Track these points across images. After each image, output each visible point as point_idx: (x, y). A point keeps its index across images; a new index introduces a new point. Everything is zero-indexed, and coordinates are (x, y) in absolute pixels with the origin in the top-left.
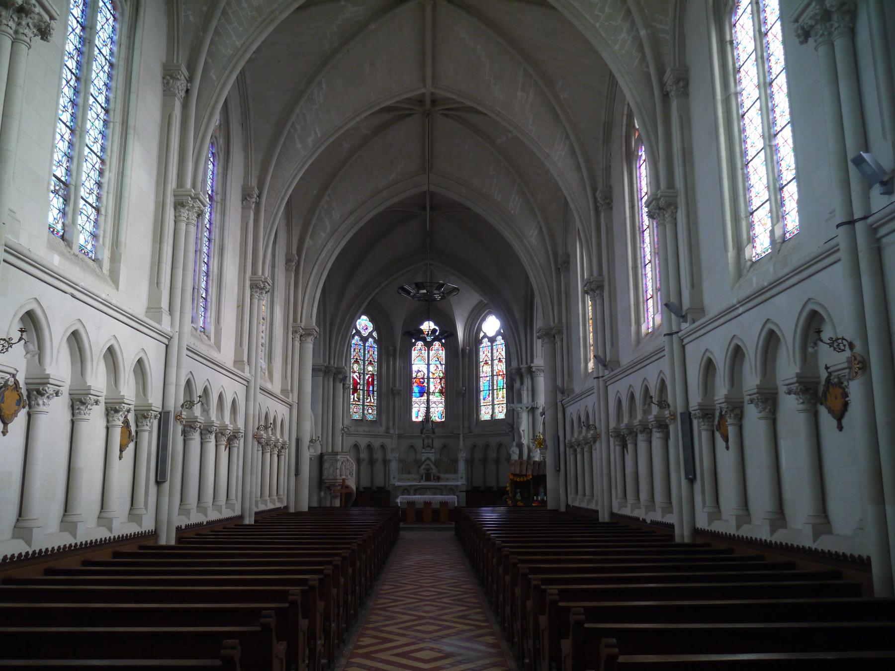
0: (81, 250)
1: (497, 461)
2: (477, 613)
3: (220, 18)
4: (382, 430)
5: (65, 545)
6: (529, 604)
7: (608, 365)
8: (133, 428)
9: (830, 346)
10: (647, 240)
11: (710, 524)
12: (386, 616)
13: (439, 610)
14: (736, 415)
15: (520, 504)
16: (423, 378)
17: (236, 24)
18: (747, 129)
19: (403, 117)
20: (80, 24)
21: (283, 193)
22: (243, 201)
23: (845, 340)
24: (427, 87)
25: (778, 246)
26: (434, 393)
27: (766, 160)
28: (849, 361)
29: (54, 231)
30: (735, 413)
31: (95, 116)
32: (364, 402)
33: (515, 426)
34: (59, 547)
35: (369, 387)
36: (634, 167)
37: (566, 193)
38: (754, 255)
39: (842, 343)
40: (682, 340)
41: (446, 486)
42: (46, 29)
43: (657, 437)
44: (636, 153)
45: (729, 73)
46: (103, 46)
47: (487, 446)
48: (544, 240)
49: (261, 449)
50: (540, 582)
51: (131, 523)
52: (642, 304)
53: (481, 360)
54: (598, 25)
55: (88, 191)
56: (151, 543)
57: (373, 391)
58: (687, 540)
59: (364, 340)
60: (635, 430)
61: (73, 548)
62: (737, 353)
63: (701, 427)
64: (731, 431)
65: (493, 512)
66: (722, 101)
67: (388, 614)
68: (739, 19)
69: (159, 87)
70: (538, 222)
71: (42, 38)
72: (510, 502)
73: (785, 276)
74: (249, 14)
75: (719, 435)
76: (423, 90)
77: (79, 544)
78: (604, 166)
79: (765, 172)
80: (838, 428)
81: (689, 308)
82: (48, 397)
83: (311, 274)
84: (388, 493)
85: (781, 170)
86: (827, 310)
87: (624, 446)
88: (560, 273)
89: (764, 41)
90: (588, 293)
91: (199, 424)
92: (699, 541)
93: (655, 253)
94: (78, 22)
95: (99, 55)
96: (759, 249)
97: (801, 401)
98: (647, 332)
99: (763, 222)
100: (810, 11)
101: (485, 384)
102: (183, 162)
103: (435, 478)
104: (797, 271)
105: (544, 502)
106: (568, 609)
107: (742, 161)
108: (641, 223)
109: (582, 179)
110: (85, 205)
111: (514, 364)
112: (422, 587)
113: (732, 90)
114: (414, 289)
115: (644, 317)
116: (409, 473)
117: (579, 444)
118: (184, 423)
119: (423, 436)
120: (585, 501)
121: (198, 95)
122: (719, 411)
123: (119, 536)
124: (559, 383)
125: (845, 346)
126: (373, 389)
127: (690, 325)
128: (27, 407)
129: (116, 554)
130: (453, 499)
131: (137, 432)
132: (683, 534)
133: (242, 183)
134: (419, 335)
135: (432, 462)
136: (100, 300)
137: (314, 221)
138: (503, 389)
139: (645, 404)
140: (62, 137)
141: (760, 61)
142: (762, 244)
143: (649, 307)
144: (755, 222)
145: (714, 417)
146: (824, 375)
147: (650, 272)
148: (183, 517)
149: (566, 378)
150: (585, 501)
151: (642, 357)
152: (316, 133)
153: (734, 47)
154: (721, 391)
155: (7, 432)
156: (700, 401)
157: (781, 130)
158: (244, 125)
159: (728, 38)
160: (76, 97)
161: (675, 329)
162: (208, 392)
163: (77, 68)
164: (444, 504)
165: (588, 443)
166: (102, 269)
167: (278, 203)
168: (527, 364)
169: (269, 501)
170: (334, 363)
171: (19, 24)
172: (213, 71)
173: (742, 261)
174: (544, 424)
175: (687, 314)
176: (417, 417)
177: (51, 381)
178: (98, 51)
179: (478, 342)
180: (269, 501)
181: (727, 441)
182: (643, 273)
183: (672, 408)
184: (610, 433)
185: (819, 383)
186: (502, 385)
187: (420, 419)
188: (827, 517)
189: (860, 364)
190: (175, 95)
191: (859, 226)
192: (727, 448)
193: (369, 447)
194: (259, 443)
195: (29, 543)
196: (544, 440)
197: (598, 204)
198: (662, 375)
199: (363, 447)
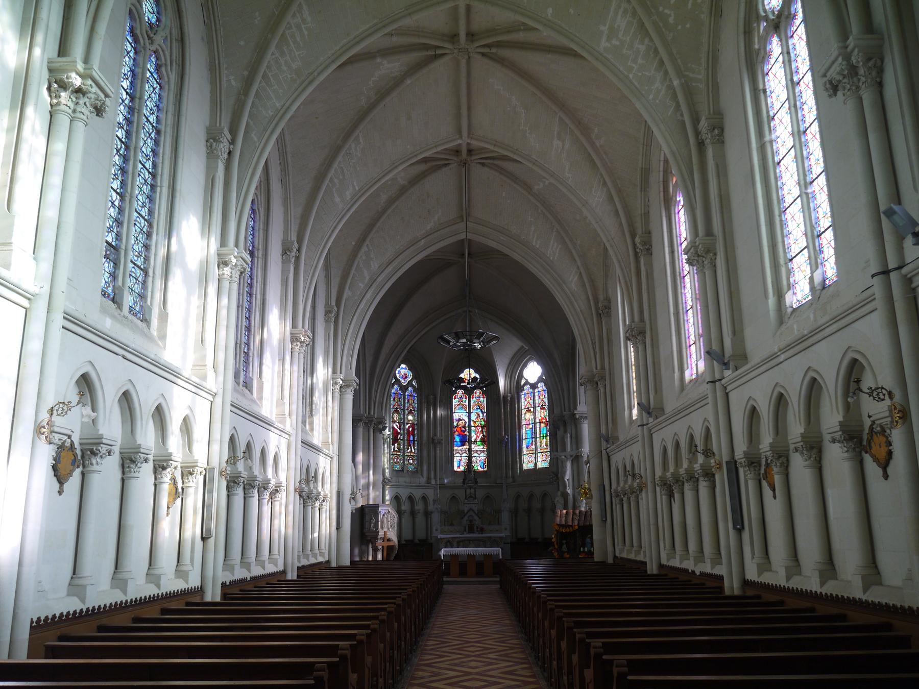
0: (131, 312)
1: (542, 511)
2: (523, 669)
3: (261, 80)
4: (423, 480)
5: (116, 603)
6: (575, 658)
8: (180, 485)
9: (870, 396)
10: (688, 286)
11: (759, 575)
12: (432, 672)
13: (485, 666)
14: (782, 464)
15: (566, 555)
16: (464, 427)
18: (783, 175)
19: (440, 167)
20: (129, 96)
21: (322, 247)
23: (885, 389)
24: (463, 138)
25: (818, 292)
26: (475, 442)
27: (802, 207)
28: (891, 409)
29: (105, 294)
30: (780, 462)
31: (143, 181)
32: (404, 452)
33: (559, 475)
34: (111, 604)
35: (410, 437)
36: (673, 212)
37: (604, 240)
38: (795, 301)
39: (882, 392)
40: (651, 430)
42: (101, 106)
43: (703, 485)
44: (674, 199)
45: (763, 122)
46: (151, 114)
47: (531, 496)
48: (584, 285)
49: (302, 502)
50: (585, 636)
51: (178, 580)
53: (523, 407)
54: (631, 76)
55: (137, 254)
56: (197, 599)
58: (737, 592)
59: (404, 389)
60: (681, 479)
61: (123, 605)
62: (780, 401)
63: (747, 475)
64: (778, 479)
65: (538, 564)
66: (757, 148)
67: (434, 670)
68: (796, 30)
69: (203, 150)
70: (578, 268)
71: (97, 115)
72: (556, 554)
73: (824, 324)
74: (289, 76)
75: (766, 484)
76: (459, 141)
77: (129, 601)
78: (643, 212)
79: (802, 219)
80: (883, 476)
81: (732, 356)
82: (101, 457)
83: (350, 325)
84: (431, 544)
85: (818, 218)
86: (867, 360)
87: (671, 496)
88: (601, 318)
89: (797, 90)
90: (629, 340)
91: (242, 479)
92: (750, 593)
93: (695, 299)
94: (127, 93)
95: (146, 123)
96: (799, 296)
97: (846, 449)
98: (691, 378)
99: (802, 268)
100: (836, 68)
101: (528, 432)
102: (226, 222)
104: (836, 319)
105: (591, 554)
106: (611, 662)
107: (779, 208)
109: (621, 224)
110: (133, 267)
111: (557, 411)
112: (467, 642)
113: (767, 138)
114: (453, 338)
115: (687, 364)
116: (452, 525)
117: (626, 494)
118: (228, 478)
119: (465, 486)
120: (633, 552)
122: (764, 459)
123: (166, 592)
124: (603, 431)
125: (884, 395)
127: (733, 372)
128: (81, 467)
129: (164, 611)
130: (497, 551)
131: (183, 489)
132: (732, 586)
133: (282, 238)
134: (457, 383)
135: (474, 512)
136: (149, 360)
137: (353, 271)
138: (546, 436)
139: (690, 452)
140: (113, 203)
141: (793, 109)
142: (802, 291)
143: (692, 353)
144: (795, 268)
145: (760, 466)
146: (867, 423)
147: (692, 318)
148: (227, 573)
149: (610, 425)
150: (633, 552)
151: (686, 405)
152: (354, 186)
154: (766, 440)
155: (63, 491)
156: (745, 449)
157: (817, 178)
158: (283, 181)
159: (761, 87)
160: (126, 165)
161: (717, 376)
163: (126, 137)
164: (487, 556)
165: (634, 492)
166: (149, 329)
168: (570, 411)
169: (310, 556)
170: (374, 414)
171: (77, 103)
172: (254, 132)
173: (783, 307)
174: (589, 472)
175: (729, 361)
176: (459, 467)
177: (104, 441)
178: (145, 120)
179: (519, 388)
180: (318, 555)
181: (774, 490)
182: (685, 318)
184: (657, 482)
185: (862, 431)
186: (545, 432)
187: (462, 468)
188: (876, 567)
189: (901, 413)
190: (218, 157)
191: (893, 275)
192: (775, 497)
193: (411, 498)
194: (300, 496)
195: (83, 601)
196: (590, 489)
197: (638, 250)
198: (706, 423)
199: (404, 499)
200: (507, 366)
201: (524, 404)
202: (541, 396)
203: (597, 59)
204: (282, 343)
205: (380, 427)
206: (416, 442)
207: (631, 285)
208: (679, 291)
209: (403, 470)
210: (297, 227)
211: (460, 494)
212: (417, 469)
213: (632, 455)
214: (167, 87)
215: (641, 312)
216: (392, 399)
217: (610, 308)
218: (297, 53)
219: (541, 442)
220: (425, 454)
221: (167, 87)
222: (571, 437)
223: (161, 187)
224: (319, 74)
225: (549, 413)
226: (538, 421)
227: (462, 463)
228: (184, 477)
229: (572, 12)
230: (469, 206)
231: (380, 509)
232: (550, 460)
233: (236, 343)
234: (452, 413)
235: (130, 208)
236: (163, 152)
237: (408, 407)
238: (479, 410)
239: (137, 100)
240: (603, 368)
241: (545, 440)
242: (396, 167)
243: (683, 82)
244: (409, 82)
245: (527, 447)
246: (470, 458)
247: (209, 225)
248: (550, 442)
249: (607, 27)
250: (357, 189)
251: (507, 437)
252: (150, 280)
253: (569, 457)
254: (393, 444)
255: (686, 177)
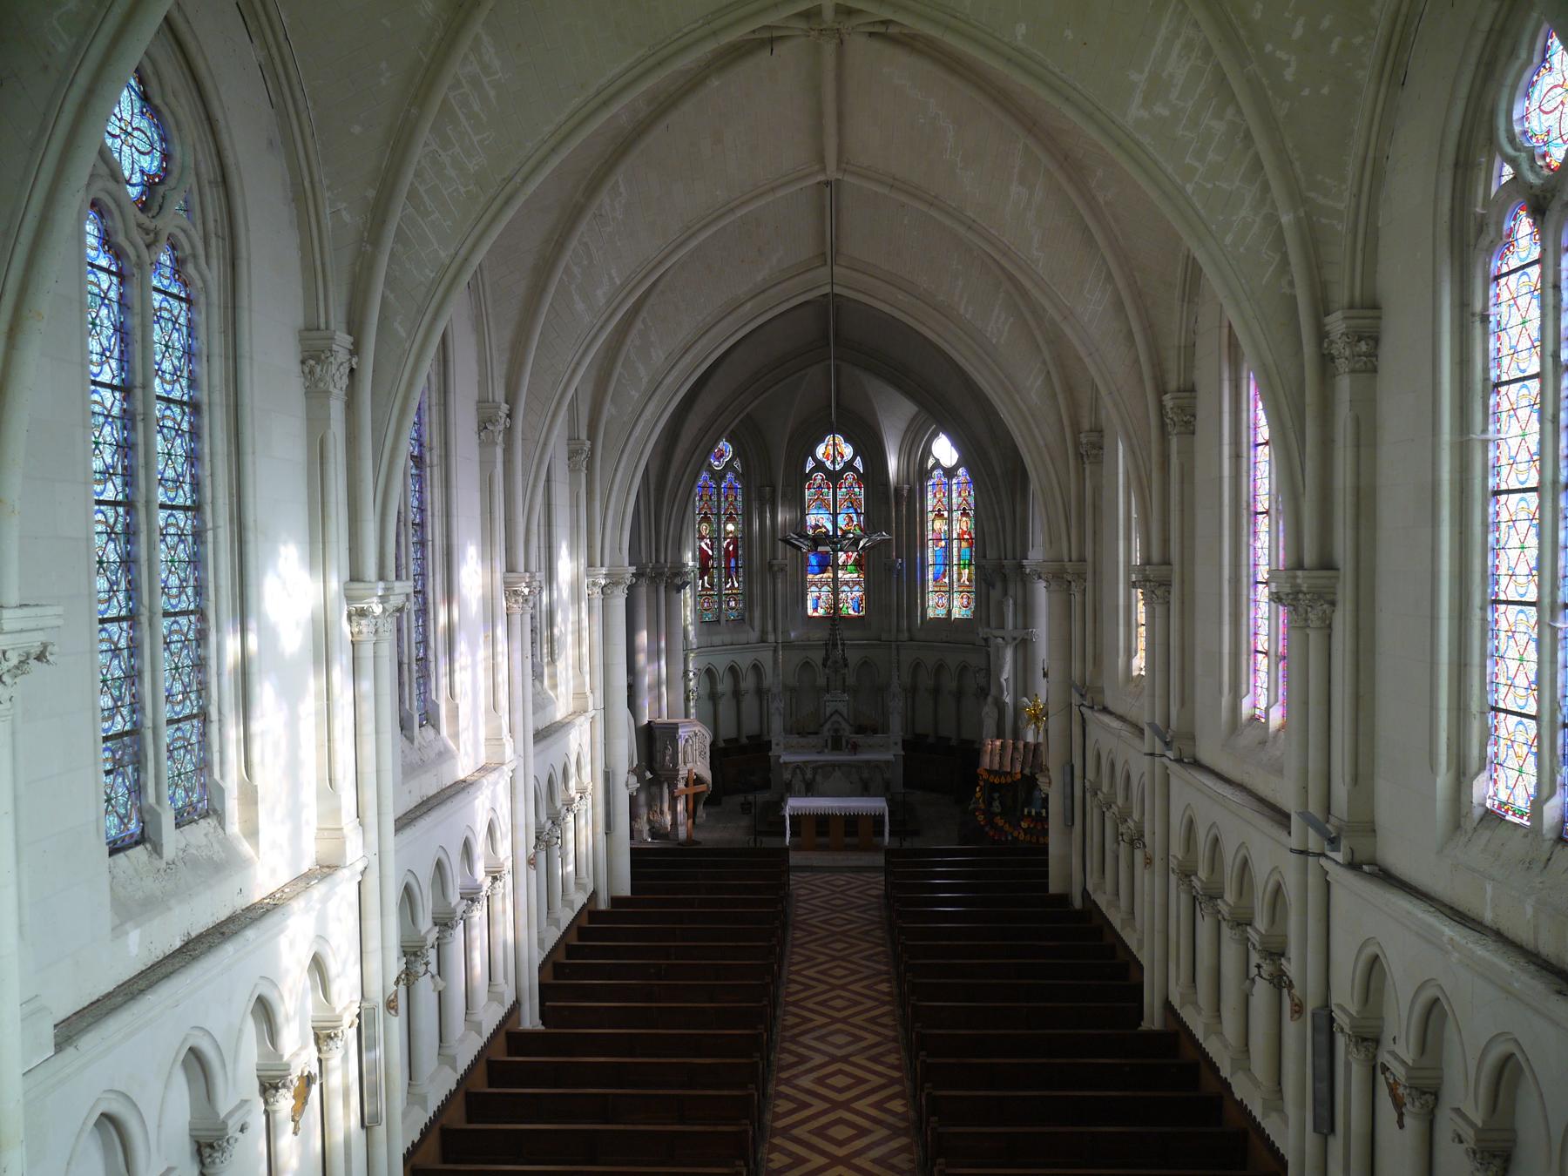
4: (754, 636)
7: (1172, 741)
17: (437, 214)
22: (480, 431)
26: (845, 566)
32: (720, 590)
41: (868, 762)
47: (940, 668)
52: (1244, 657)
53: (930, 509)
54: (1189, 188)
57: (737, 567)
74: (462, 190)
78: (1183, 345)
88: (1084, 463)
103: (849, 746)
107: (1484, 592)
108: (1252, 494)
109: (1137, 361)
113: (1477, 435)
121: (374, 371)
126: (737, 563)
137: (618, 369)
138: (970, 564)
152: (611, 278)
153: (1491, 331)
159: (1478, 307)
162: (444, 868)
166: (223, 829)
167: (547, 422)
170: (666, 561)
176: (815, 610)
179: (924, 474)
182: (1252, 596)
183: (1296, 991)
186: (968, 557)
187: (821, 612)
199: (721, 673)
200: (900, 440)
201: (931, 502)
202: (961, 493)
203: (1119, 145)
204: (489, 604)
205: (678, 581)
206: (741, 570)
207: (1150, 487)
208: (1244, 539)
209: (718, 621)
210: (505, 366)
211: (817, 657)
212: (743, 615)
213: (1126, 761)
214: (202, 299)
215: (1166, 541)
216: (697, 498)
217: (1101, 448)
218: (475, 139)
219: (960, 574)
220: (757, 590)
221: (202, 299)
222: (1015, 604)
223: (215, 528)
224: (525, 180)
225: (976, 524)
226: (955, 536)
227: (821, 603)
228: (321, 1041)
229: (1071, 37)
230: (837, 238)
231: (680, 731)
232: (976, 607)
233: (400, 664)
234: (804, 515)
235: (152, 637)
236: (211, 449)
237: (726, 510)
238: (851, 511)
239: (138, 393)
240: (1082, 559)
241: (967, 571)
242: (693, 235)
243: (1302, 214)
244: (717, 83)
245: (935, 580)
246: (835, 592)
247: (324, 543)
248: (976, 574)
249: (1146, 74)
250: (618, 282)
251: (900, 560)
252: (214, 728)
253: (1010, 640)
254: (701, 578)
255: (1289, 424)
